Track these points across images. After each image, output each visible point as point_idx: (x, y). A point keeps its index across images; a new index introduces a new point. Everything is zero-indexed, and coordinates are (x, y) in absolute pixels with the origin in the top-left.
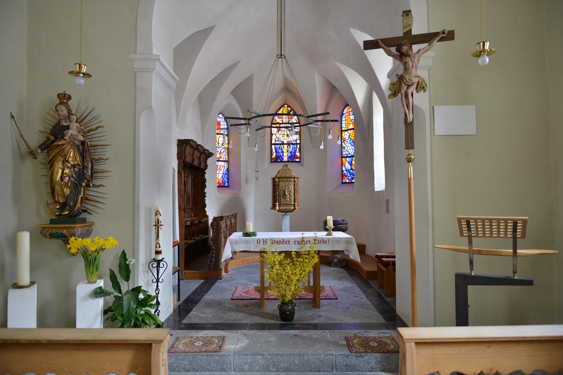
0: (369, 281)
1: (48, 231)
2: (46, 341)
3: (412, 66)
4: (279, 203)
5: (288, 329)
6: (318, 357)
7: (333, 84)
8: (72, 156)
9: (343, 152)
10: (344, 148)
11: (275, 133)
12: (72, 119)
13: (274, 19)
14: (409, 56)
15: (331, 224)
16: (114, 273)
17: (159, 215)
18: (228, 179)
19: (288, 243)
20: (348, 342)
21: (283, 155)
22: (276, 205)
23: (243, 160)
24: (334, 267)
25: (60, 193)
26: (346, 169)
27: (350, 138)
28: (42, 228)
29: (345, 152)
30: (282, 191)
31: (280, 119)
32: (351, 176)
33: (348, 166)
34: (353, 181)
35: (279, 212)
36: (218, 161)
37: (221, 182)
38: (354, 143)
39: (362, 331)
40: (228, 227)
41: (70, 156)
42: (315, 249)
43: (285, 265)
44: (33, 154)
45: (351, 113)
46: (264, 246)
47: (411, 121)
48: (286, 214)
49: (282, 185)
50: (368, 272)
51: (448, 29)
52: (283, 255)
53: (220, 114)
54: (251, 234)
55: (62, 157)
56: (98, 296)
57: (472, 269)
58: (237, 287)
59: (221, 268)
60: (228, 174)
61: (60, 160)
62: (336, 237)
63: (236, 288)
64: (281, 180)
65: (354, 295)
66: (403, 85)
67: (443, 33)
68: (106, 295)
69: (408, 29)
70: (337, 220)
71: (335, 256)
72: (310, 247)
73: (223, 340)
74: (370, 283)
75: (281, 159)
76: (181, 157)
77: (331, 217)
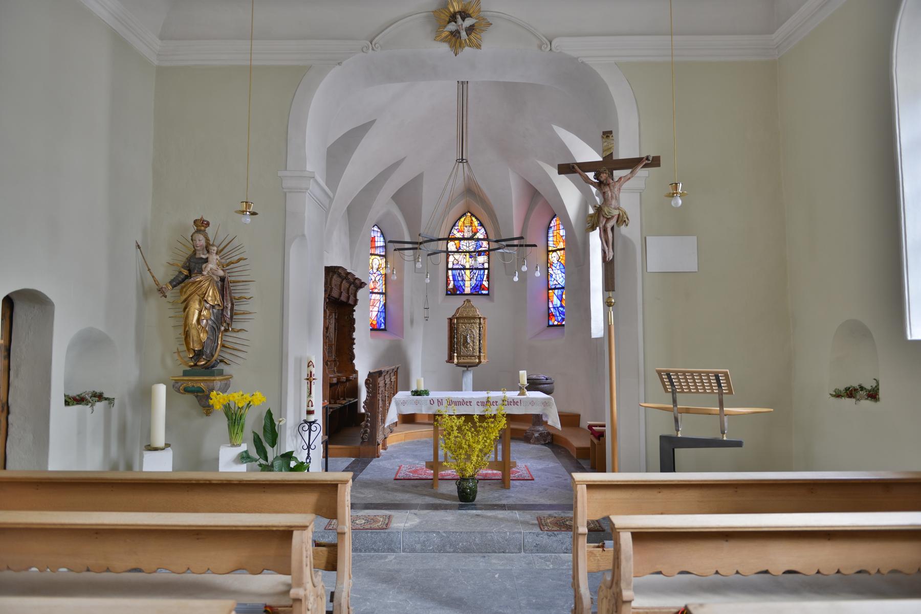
0: (579, 461)
1: (182, 384)
2: (237, 481)
3: (612, 196)
5: (469, 509)
6: (503, 535)
7: (535, 187)
8: (212, 296)
10: (552, 276)
12: (212, 251)
13: (454, 105)
14: (608, 185)
15: (524, 380)
16: (258, 436)
17: (312, 366)
18: (385, 319)
19: (469, 404)
20: (540, 521)
23: (407, 293)
24: (534, 443)
25: (195, 338)
27: (560, 262)
28: (174, 381)
30: (462, 337)
31: (460, 233)
32: (560, 316)
33: (556, 302)
34: (564, 323)
35: (458, 366)
37: (374, 323)
38: (565, 268)
39: (560, 512)
40: (387, 386)
41: (209, 295)
42: (503, 412)
43: (466, 431)
44: (161, 291)
45: (561, 227)
46: (439, 408)
47: (611, 259)
48: (467, 370)
50: (578, 449)
51: (653, 154)
52: (463, 418)
55: (199, 296)
56: (244, 462)
57: (678, 430)
58: (401, 466)
59: (378, 442)
60: (385, 312)
61: (196, 300)
62: (530, 397)
63: (400, 467)
65: (557, 475)
66: (602, 218)
67: (647, 158)
68: (253, 461)
69: (608, 153)
70: (538, 378)
72: (497, 410)
73: (389, 518)
74: (580, 464)
75: (462, 290)
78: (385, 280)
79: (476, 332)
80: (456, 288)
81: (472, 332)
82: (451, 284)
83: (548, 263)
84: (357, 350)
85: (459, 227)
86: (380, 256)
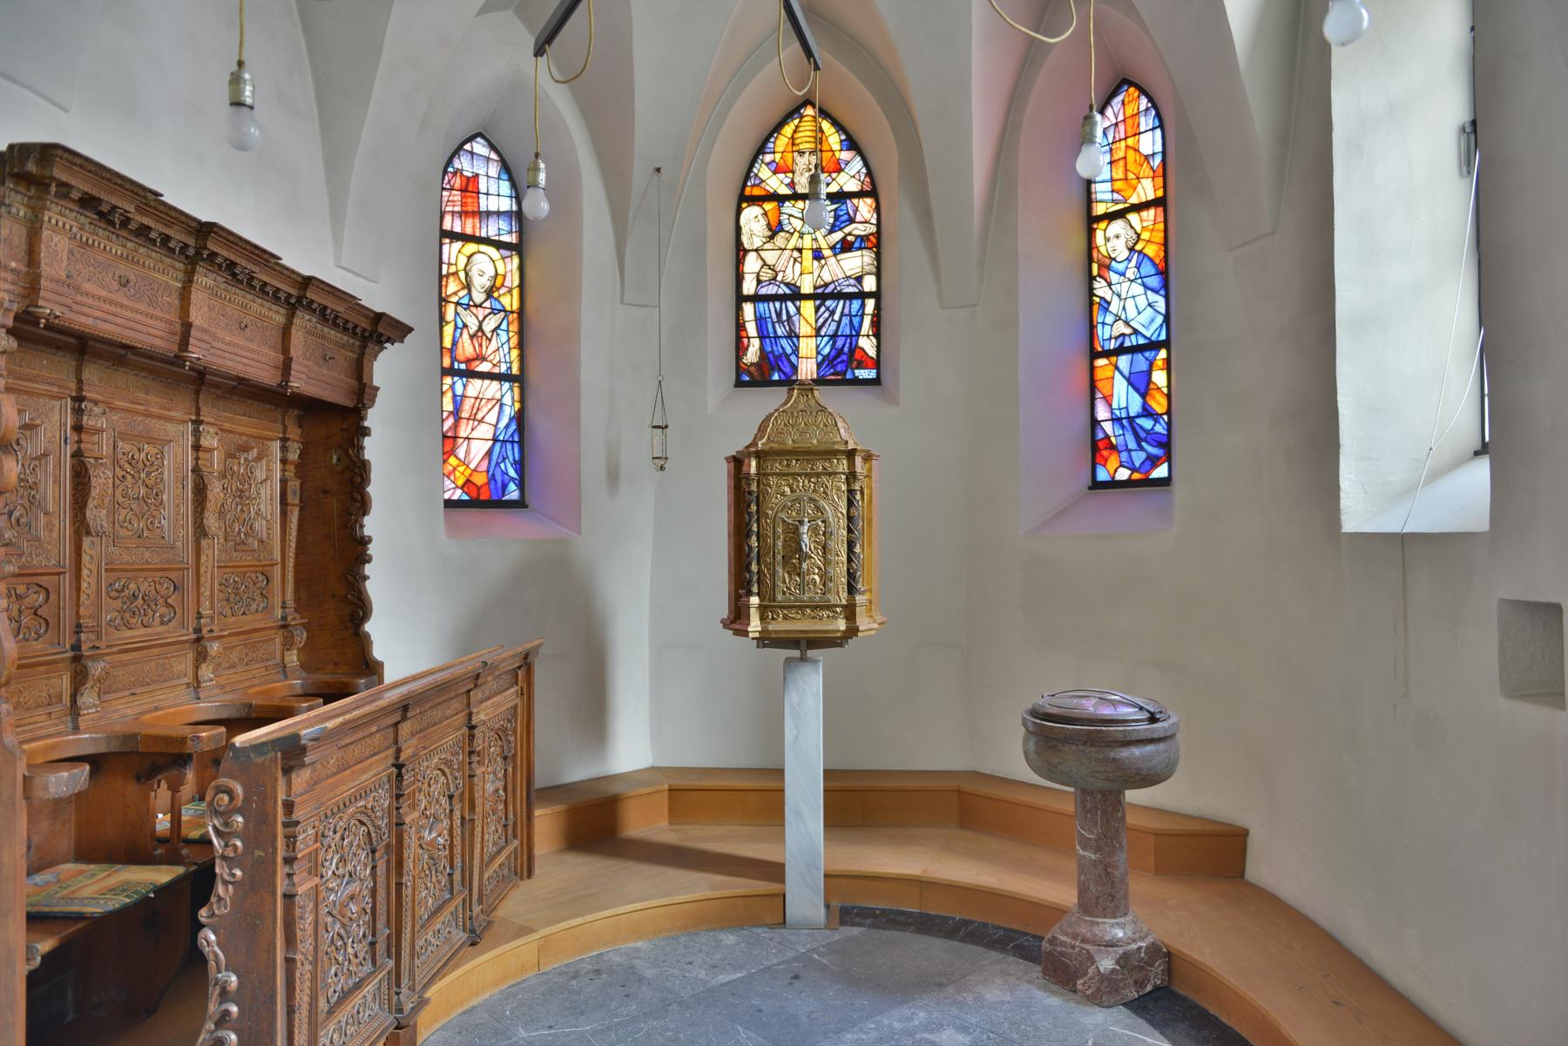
4: (762, 600)
9: (1100, 327)
10: (1105, 305)
11: (757, 243)
18: (520, 466)
22: (748, 607)
26: (1117, 412)
31: (781, 176)
33: (1123, 396)
35: (765, 646)
37: (480, 479)
48: (803, 659)
49: (783, 494)
53: (479, 139)
64: (778, 467)
71: (1096, 930)
75: (787, 370)
78: (521, 333)
80: (769, 361)
81: (818, 508)
83: (1090, 260)
84: (378, 582)
85: (778, 157)
86: (499, 245)
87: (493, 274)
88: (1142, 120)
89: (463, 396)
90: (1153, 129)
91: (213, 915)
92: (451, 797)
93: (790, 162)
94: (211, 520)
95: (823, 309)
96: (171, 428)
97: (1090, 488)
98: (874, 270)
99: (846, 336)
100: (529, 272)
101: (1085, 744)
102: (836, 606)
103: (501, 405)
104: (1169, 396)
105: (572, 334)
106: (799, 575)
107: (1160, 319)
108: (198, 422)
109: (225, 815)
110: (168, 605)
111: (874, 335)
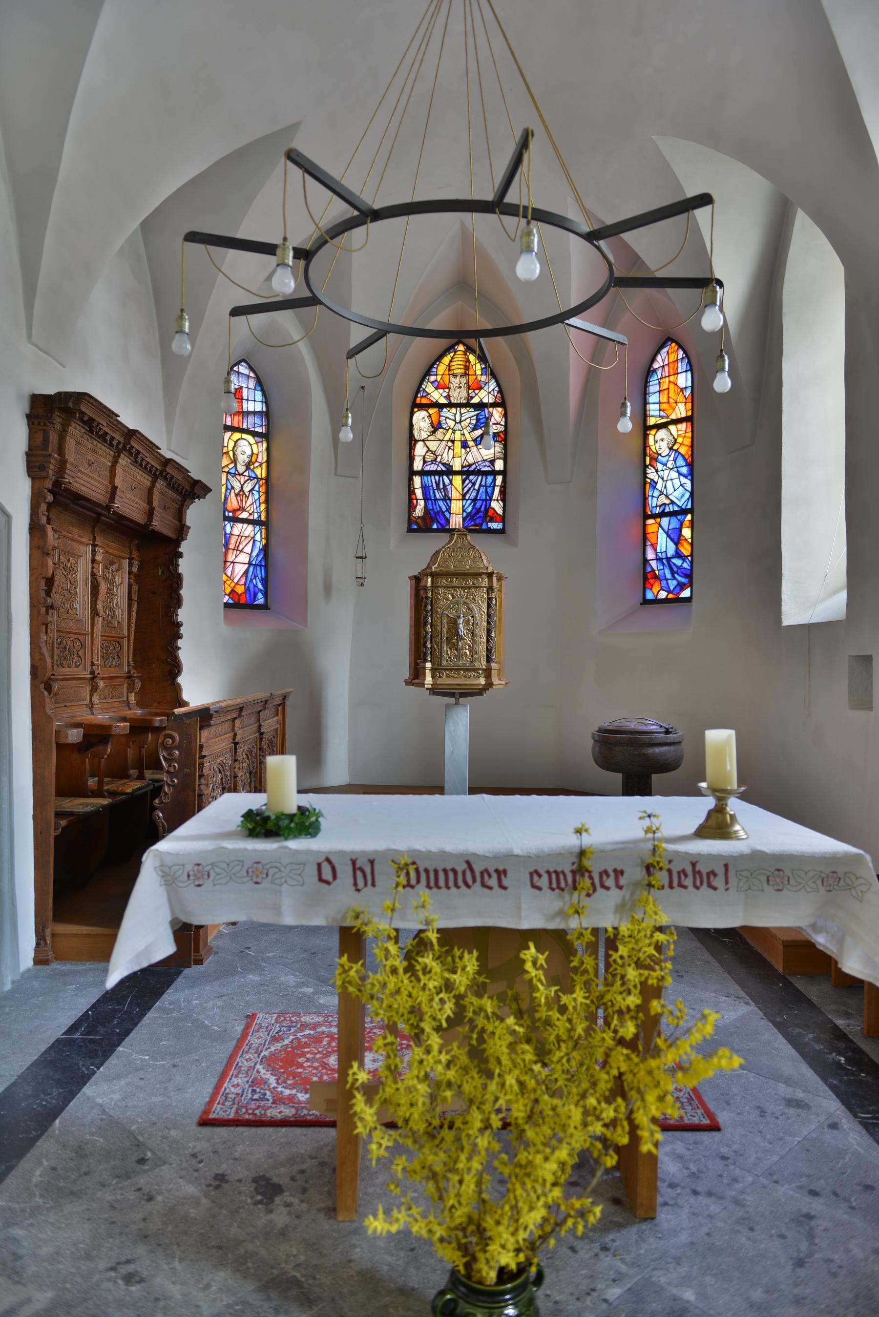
9: (650, 498)
10: (654, 484)
11: (424, 435)
18: (265, 581)
19: (493, 882)
21: (450, 507)
22: (425, 669)
23: (316, 520)
26: (660, 555)
27: (676, 451)
29: (655, 499)
31: (441, 391)
32: (675, 578)
33: (664, 544)
35: (435, 694)
36: (226, 519)
37: (240, 589)
48: (457, 703)
49: (447, 599)
54: (288, 827)
60: (266, 567)
70: (644, 728)
75: (443, 522)
76: (42, 467)
77: (729, 736)
78: (267, 493)
79: (480, 610)
81: (469, 608)
82: (418, 507)
83: (645, 455)
84: (186, 651)
86: (254, 434)
87: (250, 453)
88: (680, 365)
89: (231, 534)
90: (686, 371)
91: (162, 802)
92: (250, 773)
93: (447, 382)
94: (100, 606)
95: (467, 481)
96: (82, 548)
97: (641, 604)
98: (502, 456)
99: (483, 500)
100: (275, 453)
101: (627, 745)
102: (479, 669)
103: (254, 541)
104: (692, 544)
105: (303, 494)
106: (456, 650)
107: (687, 495)
108: (94, 546)
109: (169, 749)
110: (79, 656)
111: (501, 500)
